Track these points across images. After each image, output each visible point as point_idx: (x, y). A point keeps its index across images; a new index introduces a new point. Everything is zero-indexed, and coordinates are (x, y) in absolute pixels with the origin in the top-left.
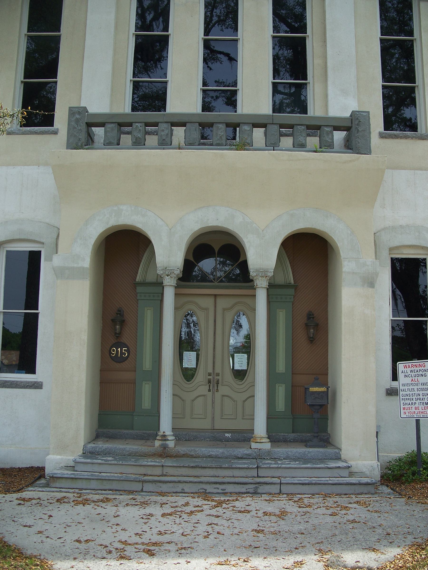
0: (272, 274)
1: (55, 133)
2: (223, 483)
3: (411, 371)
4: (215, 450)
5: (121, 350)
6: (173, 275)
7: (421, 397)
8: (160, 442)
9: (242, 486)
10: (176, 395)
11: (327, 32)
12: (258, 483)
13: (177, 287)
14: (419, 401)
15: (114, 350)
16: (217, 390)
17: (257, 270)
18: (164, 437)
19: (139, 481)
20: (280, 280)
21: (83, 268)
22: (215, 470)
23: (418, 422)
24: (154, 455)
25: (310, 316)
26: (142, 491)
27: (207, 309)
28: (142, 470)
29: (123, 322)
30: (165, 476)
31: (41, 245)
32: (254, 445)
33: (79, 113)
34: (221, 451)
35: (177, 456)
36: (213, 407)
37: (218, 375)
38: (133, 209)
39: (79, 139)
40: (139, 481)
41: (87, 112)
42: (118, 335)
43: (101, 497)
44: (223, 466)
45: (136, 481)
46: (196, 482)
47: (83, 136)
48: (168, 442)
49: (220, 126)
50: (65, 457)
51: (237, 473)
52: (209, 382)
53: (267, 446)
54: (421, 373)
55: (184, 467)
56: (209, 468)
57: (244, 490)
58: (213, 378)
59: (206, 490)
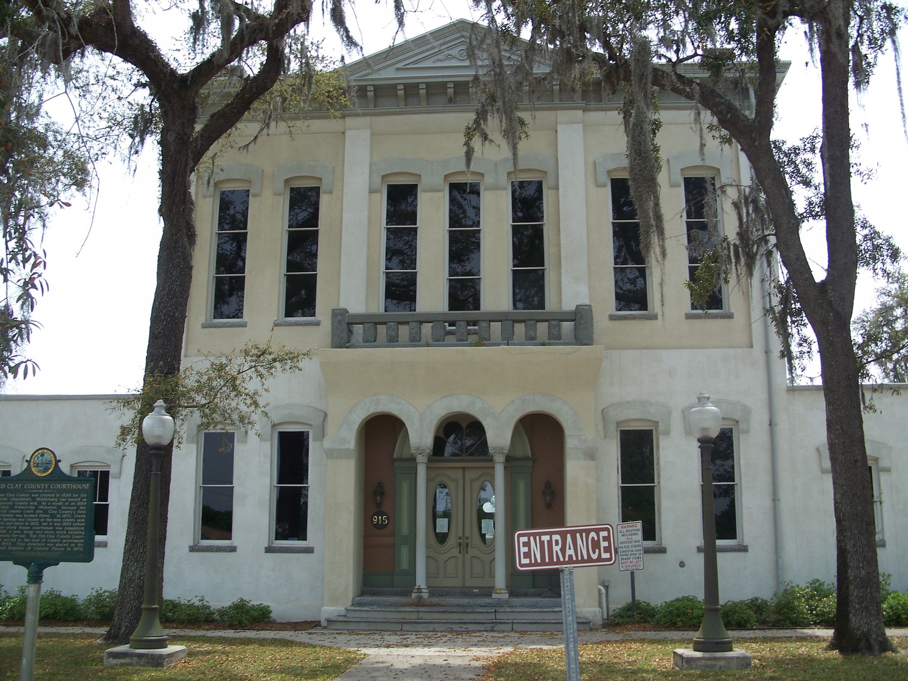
0: (507, 451)
1: (318, 324)
3: (627, 531)
4: (461, 600)
5: (382, 518)
6: (424, 454)
7: (634, 552)
8: (416, 594)
9: (481, 625)
10: (430, 557)
11: (561, 222)
12: (494, 623)
14: (632, 556)
15: (375, 519)
16: (467, 552)
17: (494, 449)
19: (399, 623)
20: (519, 453)
21: (348, 450)
22: (460, 614)
23: (632, 573)
24: (411, 605)
25: (548, 485)
26: (401, 630)
28: (402, 616)
29: (382, 494)
31: (309, 427)
33: (341, 315)
35: (431, 605)
36: (464, 567)
37: (467, 538)
39: (342, 338)
40: (399, 623)
41: (348, 312)
42: (379, 505)
44: (467, 611)
47: (344, 335)
49: (462, 323)
50: (337, 608)
52: (460, 545)
53: (506, 596)
54: (634, 532)
56: (456, 612)
58: (463, 541)
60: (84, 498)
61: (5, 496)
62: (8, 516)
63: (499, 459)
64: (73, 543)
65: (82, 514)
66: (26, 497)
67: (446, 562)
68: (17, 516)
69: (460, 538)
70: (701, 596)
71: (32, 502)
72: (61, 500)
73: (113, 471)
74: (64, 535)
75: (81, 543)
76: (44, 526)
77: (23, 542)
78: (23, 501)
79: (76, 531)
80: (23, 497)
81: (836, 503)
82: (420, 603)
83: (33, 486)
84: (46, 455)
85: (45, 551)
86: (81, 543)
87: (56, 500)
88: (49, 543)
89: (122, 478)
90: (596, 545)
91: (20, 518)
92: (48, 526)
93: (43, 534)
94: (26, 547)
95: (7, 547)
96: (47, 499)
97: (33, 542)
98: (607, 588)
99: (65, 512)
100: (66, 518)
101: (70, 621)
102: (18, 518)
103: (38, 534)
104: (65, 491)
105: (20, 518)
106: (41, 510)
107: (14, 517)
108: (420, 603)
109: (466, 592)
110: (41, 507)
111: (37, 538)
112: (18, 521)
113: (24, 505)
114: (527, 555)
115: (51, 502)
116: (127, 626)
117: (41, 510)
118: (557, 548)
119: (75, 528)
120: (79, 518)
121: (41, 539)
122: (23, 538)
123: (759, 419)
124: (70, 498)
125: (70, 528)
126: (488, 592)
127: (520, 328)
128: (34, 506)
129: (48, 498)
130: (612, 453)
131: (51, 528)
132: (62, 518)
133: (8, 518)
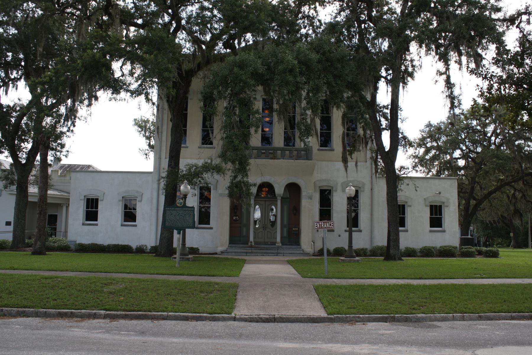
18: (251, 242)
35: (255, 247)
70: (347, 248)
81: (388, 217)
82: (251, 247)
90: (330, 225)
98: (314, 243)
108: (251, 247)
109: (266, 243)
114: (317, 226)
118: (323, 225)
123: (367, 187)
126: (274, 243)
127: (287, 152)
130: (317, 197)
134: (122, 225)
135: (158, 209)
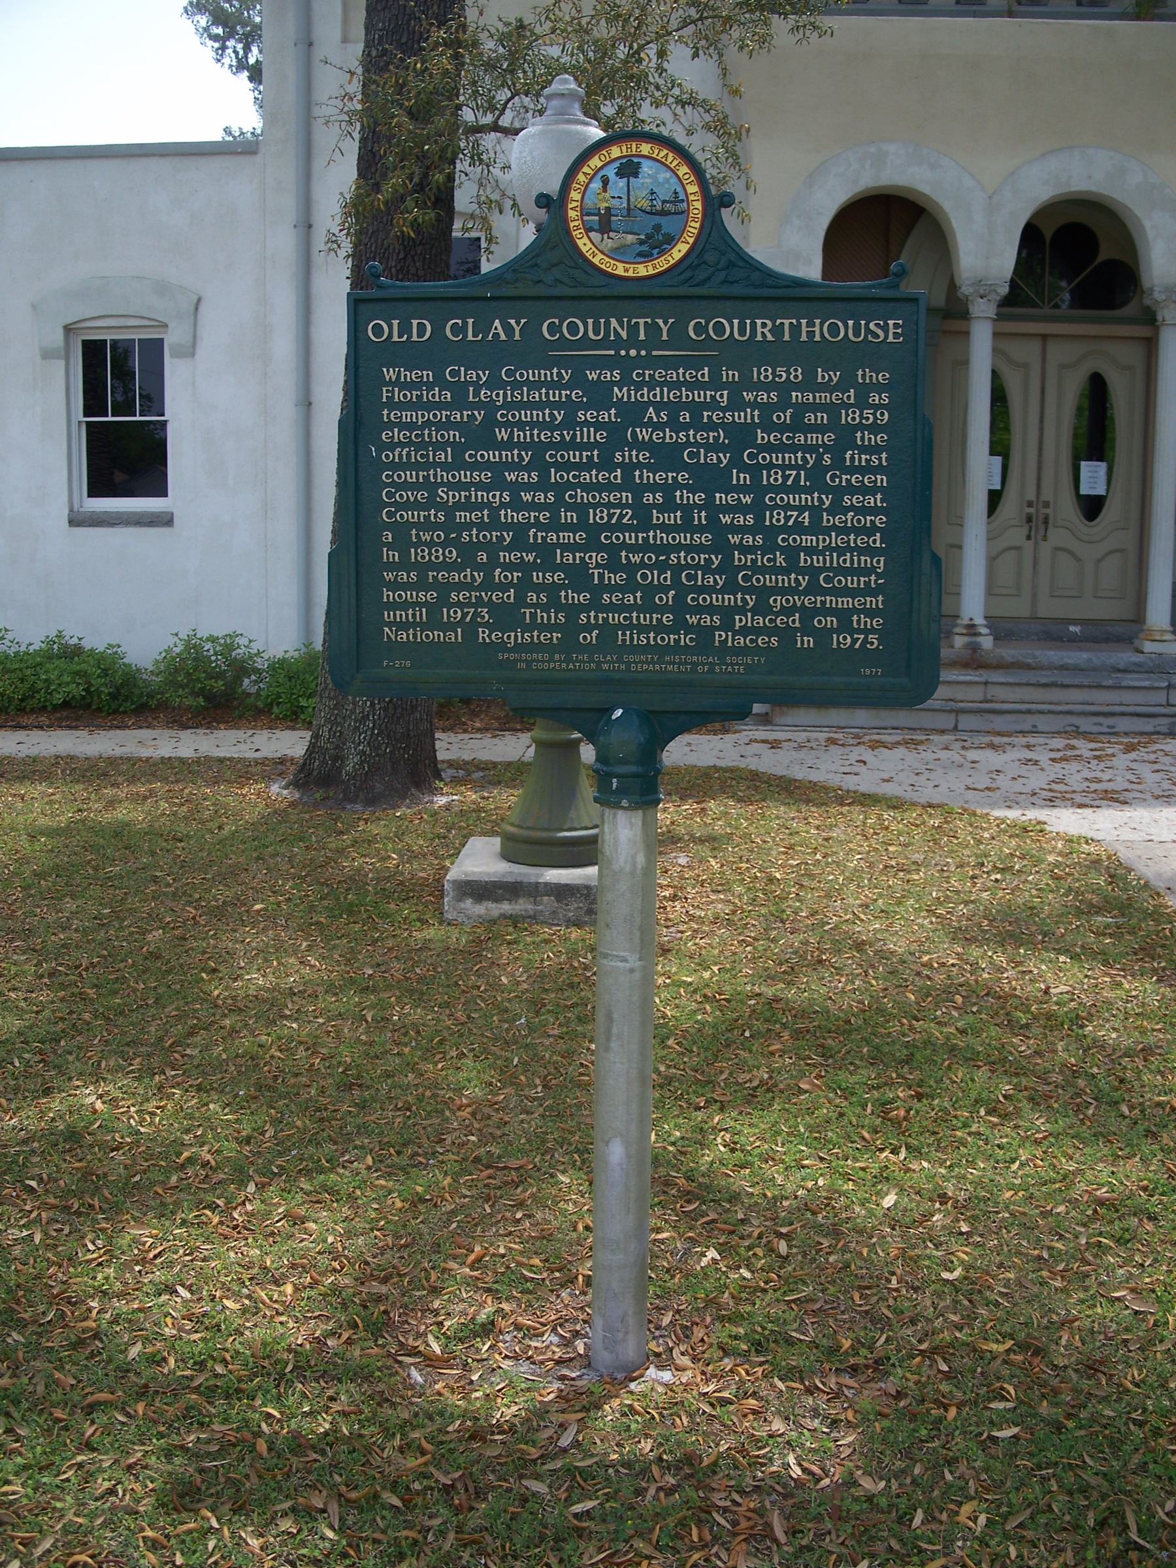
2: (1112, 714)
4: (1072, 654)
8: (966, 639)
13: (1000, 317)
16: (1045, 538)
18: (971, 628)
19: (951, 711)
22: (1086, 690)
26: (956, 728)
27: (1025, 366)
30: (991, 701)
32: (1148, 647)
34: (1085, 656)
35: (1000, 666)
37: (1047, 505)
38: (910, 150)
40: (951, 711)
43: (899, 738)
44: (1105, 683)
45: (944, 711)
46: (1060, 713)
48: (980, 639)
51: (1127, 697)
52: (1029, 519)
55: (1028, 684)
57: (1149, 728)
59: (1078, 727)
60: (879, 388)
61: (440, 381)
62: (464, 476)
63: (983, 310)
64: (825, 611)
65: (867, 469)
66: (552, 385)
67: (1099, 561)
68: (511, 477)
69: (1030, 504)
71: (586, 407)
72: (748, 396)
73: (171, 340)
74: (776, 570)
75: (871, 613)
76: (664, 528)
77: (554, 603)
78: (540, 406)
79: (841, 551)
80: (535, 385)
83: (586, 328)
84: (647, 168)
85: (677, 648)
86: (871, 613)
87: (724, 397)
88: (698, 610)
89: (200, 353)
91: (528, 487)
92: (687, 526)
93: (662, 567)
94: (571, 629)
95: (471, 629)
96: (670, 395)
97: (611, 608)
99: (777, 459)
100: (784, 489)
101: (125, 712)
102: (516, 488)
103: (631, 569)
104: (772, 353)
105: (528, 487)
106: (640, 446)
107: (499, 483)
110: (643, 434)
111: (630, 586)
112: (517, 504)
113: (550, 426)
115: (696, 409)
116: (363, 752)
117: (640, 446)
119: (835, 540)
120: (851, 490)
121: (650, 591)
122: (553, 588)
124: (797, 387)
125: (808, 540)
128: (598, 426)
129: (677, 385)
131: (704, 539)
132: (757, 489)
133: (466, 487)
134: (77, 520)
135: (306, 404)
